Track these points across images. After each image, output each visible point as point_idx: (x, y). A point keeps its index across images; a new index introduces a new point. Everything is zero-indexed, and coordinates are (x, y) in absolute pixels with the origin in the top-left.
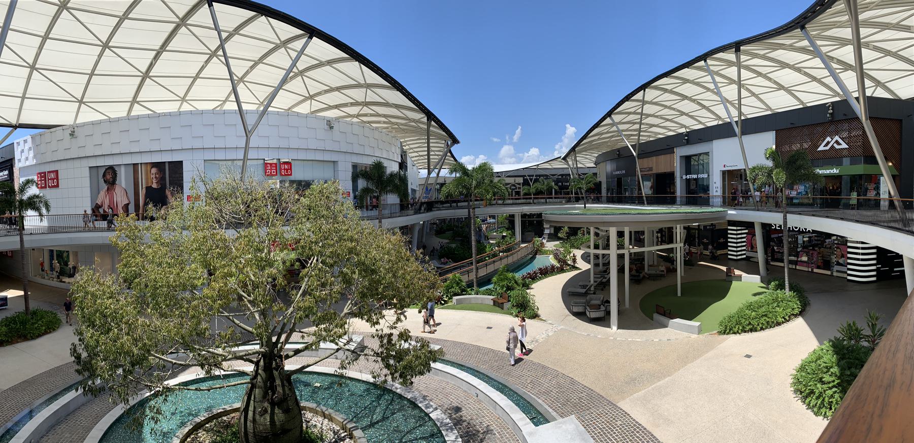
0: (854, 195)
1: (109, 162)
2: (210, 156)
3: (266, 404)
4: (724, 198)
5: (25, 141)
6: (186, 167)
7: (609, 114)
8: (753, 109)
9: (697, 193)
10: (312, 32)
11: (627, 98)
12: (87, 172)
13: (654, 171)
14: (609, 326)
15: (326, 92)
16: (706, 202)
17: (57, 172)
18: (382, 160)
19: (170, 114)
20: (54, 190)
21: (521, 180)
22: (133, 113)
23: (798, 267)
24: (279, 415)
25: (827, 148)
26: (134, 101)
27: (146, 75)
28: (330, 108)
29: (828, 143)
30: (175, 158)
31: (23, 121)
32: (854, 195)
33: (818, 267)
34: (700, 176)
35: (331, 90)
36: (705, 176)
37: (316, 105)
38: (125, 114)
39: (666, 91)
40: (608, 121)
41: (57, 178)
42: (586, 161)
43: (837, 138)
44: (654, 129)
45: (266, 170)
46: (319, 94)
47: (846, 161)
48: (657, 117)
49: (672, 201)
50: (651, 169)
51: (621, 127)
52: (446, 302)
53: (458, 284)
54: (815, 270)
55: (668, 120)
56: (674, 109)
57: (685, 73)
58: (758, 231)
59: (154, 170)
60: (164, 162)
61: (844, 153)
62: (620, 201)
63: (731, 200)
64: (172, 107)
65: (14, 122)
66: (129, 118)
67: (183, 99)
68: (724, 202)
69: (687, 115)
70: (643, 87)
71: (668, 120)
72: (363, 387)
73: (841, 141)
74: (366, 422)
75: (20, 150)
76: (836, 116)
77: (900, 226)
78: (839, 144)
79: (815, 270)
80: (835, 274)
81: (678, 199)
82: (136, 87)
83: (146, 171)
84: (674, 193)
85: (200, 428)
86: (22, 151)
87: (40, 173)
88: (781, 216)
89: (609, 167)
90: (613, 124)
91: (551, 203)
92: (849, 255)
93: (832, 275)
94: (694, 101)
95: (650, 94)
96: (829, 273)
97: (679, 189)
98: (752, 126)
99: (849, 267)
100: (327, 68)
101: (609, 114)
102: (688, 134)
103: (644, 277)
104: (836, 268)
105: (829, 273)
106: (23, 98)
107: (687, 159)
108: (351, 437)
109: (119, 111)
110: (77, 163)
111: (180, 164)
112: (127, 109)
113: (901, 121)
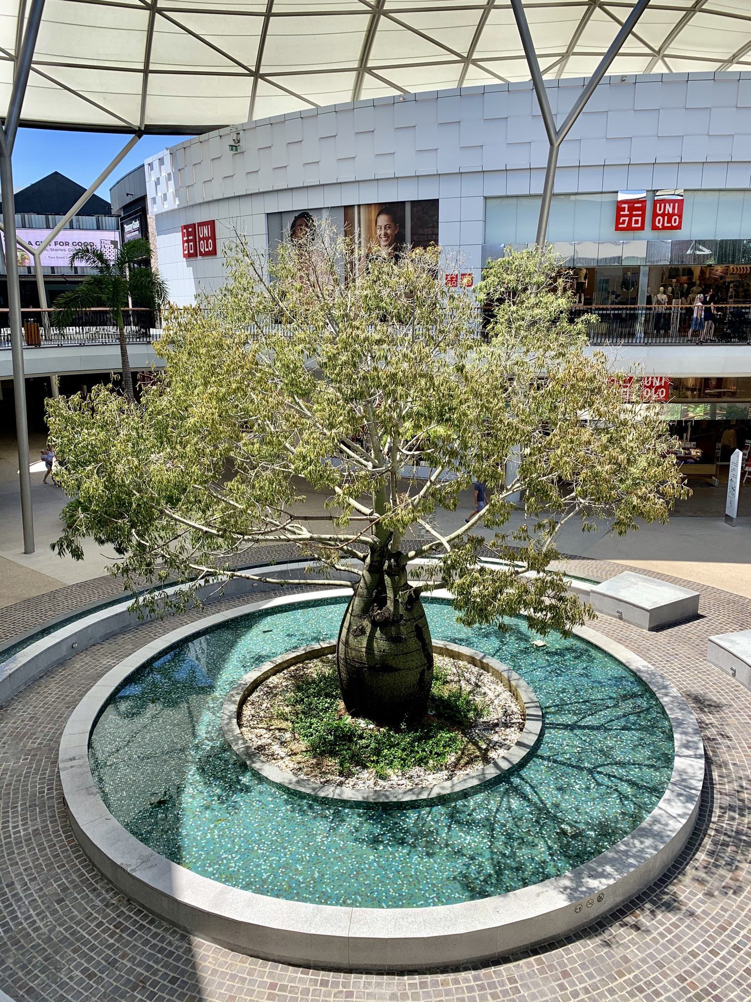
1: (300, 203)
2: (496, 187)
3: (366, 623)
5: (161, 161)
6: (444, 214)
12: (261, 225)
17: (212, 224)
19: (437, 97)
20: (209, 260)
22: (364, 96)
24: (381, 644)
26: (363, 68)
30: (424, 194)
31: (155, 117)
38: (347, 98)
41: (213, 237)
45: (618, 216)
59: (383, 220)
60: (404, 202)
64: (444, 79)
65: (135, 122)
66: (355, 106)
75: (153, 179)
82: (363, 36)
83: (369, 221)
85: (316, 658)
86: (157, 183)
87: (186, 227)
106: (146, 71)
109: (336, 91)
110: (246, 204)
111: (434, 204)
112: (351, 86)
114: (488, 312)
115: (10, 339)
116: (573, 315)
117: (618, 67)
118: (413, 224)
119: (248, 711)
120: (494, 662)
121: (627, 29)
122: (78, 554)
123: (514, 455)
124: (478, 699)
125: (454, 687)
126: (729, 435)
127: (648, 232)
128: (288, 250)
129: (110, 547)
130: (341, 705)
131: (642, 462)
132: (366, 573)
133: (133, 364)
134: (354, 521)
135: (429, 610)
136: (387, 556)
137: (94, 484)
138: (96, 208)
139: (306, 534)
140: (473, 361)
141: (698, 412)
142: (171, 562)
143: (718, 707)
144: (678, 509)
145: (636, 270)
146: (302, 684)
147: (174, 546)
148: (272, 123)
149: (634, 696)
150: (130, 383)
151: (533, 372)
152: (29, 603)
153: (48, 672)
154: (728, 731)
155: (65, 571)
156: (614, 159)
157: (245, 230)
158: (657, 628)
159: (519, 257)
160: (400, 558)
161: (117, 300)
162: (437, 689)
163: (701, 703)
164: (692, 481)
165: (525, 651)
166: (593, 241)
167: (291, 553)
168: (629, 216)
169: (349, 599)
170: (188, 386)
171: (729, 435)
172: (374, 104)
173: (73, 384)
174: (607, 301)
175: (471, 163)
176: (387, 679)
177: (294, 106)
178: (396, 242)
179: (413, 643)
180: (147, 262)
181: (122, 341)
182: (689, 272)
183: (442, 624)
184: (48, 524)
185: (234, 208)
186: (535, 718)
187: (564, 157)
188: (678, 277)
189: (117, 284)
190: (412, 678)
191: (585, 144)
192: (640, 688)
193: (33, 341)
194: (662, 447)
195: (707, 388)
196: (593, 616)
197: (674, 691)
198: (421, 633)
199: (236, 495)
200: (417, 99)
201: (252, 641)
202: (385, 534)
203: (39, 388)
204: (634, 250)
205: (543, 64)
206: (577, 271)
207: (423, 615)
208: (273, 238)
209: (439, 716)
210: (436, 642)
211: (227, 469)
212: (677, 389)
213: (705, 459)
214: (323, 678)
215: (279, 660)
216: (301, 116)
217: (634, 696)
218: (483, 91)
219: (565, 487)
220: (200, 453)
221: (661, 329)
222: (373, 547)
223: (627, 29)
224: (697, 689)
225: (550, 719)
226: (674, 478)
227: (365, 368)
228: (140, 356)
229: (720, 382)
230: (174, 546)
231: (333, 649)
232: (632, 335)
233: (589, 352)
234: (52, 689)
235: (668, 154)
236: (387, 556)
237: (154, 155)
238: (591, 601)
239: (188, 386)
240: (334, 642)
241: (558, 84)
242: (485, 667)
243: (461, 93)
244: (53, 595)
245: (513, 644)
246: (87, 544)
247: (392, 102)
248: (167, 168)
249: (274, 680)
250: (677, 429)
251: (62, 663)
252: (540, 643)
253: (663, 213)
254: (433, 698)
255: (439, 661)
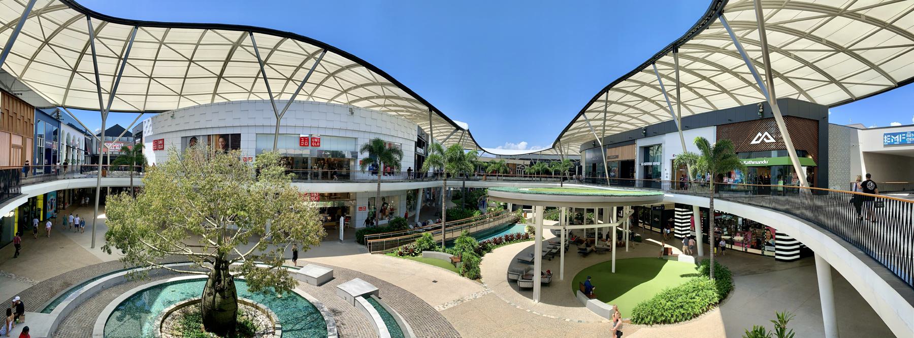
0: (781, 183)
1: (193, 134)
2: (260, 131)
4: (673, 183)
7: (583, 112)
8: (700, 107)
9: (651, 179)
10: (326, 48)
11: (595, 99)
12: (179, 140)
13: (620, 159)
14: (532, 298)
15: (355, 88)
16: (658, 186)
18: (382, 138)
19: (241, 102)
21: (528, 162)
22: (215, 101)
23: (734, 247)
25: (758, 142)
26: (215, 93)
27: (220, 77)
28: (361, 99)
29: (759, 138)
30: (236, 131)
31: (148, 108)
32: (781, 183)
33: (752, 247)
34: (655, 164)
35: (357, 87)
36: (658, 164)
37: (351, 98)
39: (627, 93)
40: (582, 118)
42: (573, 150)
43: (766, 133)
44: (623, 125)
46: (350, 89)
47: (774, 153)
48: (624, 115)
49: (630, 184)
50: (617, 157)
51: (593, 123)
52: (416, 254)
53: (428, 241)
54: (749, 250)
55: (633, 118)
56: (637, 109)
57: (639, 76)
58: (696, 213)
59: (221, 140)
61: (773, 147)
62: (594, 182)
63: (680, 185)
64: (243, 97)
65: (142, 109)
66: (212, 104)
67: (310, 95)
68: (673, 187)
69: (649, 113)
70: (606, 90)
71: (633, 118)
72: (305, 304)
73: (769, 136)
74: (289, 327)
76: (758, 117)
77: (809, 214)
78: (768, 139)
79: (749, 250)
80: (766, 253)
81: (637, 182)
84: (633, 176)
88: (708, 200)
89: (589, 156)
90: (588, 121)
91: (550, 182)
92: (777, 237)
93: (763, 255)
94: (653, 102)
95: (613, 95)
96: (759, 252)
97: (638, 174)
98: (692, 122)
99: (777, 247)
100: (347, 71)
101: (583, 112)
102: (646, 129)
103: (592, 251)
104: (767, 248)
105: (759, 252)
106: (147, 95)
107: (646, 149)
108: (274, 334)
109: (207, 100)
110: (175, 134)
113: (818, 121)
114: (258, 171)
115: (97, 174)
116: (287, 173)
117: (298, 98)
118: (232, 142)
119: (164, 325)
120: (261, 306)
121: (300, 87)
122: (109, 252)
123: (269, 222)
124: (255, 323)
125: (245, 317)
126: (339, 211)
127: (310, 147)
128: (189, 150)
129: (120, 250)
130: (202, 325)
131: (311, 224)
132: (213, 269)
133: (134, 184)
134: (211, 248)
135: (237, 284)
136: (221, 263)
137: (118, 227)
138: (128, 134)
139: (191, 253)
140: (252, 188)
141: (329, 205)
142: (140, 259)
143: (340, 313)
144: (323, 239)
145: (307, 159)
146: (186, 315)
147: (142, 253)
148: (184, 109)
149: (312, 313)
150: (134, 191)
151: (274, 191)
152: (90, 267)
153: (93, 296)
154: (345, 322)
155: (105, 257)
156: (299, 124)
157: (174, 143)
158: (320, 285)
159: (267, 154)
160: (227, 263)
161: (131, 163)
162: (240, 319)
163: (335, 312)
164: (327, 228)
165: (274, 300)
166: (293, 149)
167: (186, 259)
168: (304, 142)
169: (206, 279)
170: (152, 194)
171: (339, 211)
172: (218, 104)
173: (117, 190)
174: (297, 168)
175: (251, 123)
176: (222, 315)
177: (192, 104)
178: (226, 147)
179: (231, 299)
180: (141, 151)
181: (131, 176)
182: (323, 159)
183: (241, 289)
184: (101, 242)
185: (170, 135)
186: (279, 329)
187: (282, 122)
188: (320, 161)
189: (132, 158)
190: (231, 315)
191: (289, 119)
192: (314, 309)
193: (104, 175)
194: (317, 219)
195: (331, 196)
196: (297, 283)
197: (326, 309)
198: (234, 294)
199: (165, 235)
200: (233, 103)
201: (166, 294)
202: (221, 253)
203: (104, 190)
204: (306, 152)
205: (274, 95)
206: (287, 158)
207: (234, 287)
208: (184, 146)
209: (240, 331)
210: (239, 298)
211: (163, 226)
212: (322, 197)
213: (332, 220)
214: (196, 314)
215: (178, 304)
216: (194, 107)
217: (312, 313)
218: (256, 102)
219: (287, 234)
220: (154, 219)
221: (315, 177)
222: (216, 258)
223: (300, 87)
224: (334, 307)
225: (284, 329)
226: (322, 230)
227: (215, 190)
228: (137, 181)
229: (335, 194)
230: (142, 253)
231: (199, 301)
232: (307, 179)
233: (292, 185)
234: (94, 303)
235: (315, 124)
236: (221, 263)
237: (147, 120)
238: (298, 277)
239: (152, 194)
240: (200, 297)
241: (279, 101)
242: (257, 308)
243: (248, 102)
244: (98, 265)
245: (269, 297)
246: (113, 249)
247: (225, 103)
248: (150, 123)
249: (175, 313)
250: (322, 211)
251: (98, 293)
252: (279, 296)
253: (315, 142)
254: (237, 323)
255: (241, 306)
